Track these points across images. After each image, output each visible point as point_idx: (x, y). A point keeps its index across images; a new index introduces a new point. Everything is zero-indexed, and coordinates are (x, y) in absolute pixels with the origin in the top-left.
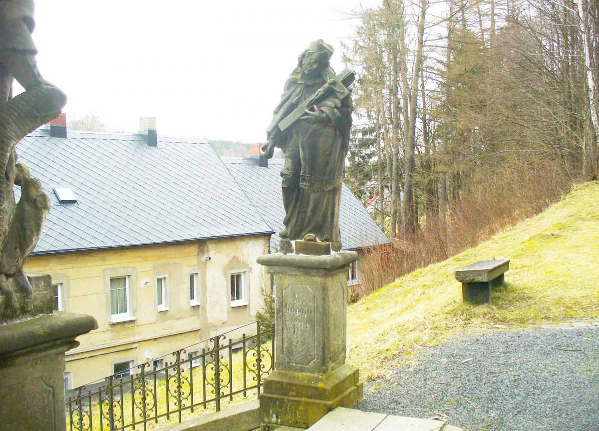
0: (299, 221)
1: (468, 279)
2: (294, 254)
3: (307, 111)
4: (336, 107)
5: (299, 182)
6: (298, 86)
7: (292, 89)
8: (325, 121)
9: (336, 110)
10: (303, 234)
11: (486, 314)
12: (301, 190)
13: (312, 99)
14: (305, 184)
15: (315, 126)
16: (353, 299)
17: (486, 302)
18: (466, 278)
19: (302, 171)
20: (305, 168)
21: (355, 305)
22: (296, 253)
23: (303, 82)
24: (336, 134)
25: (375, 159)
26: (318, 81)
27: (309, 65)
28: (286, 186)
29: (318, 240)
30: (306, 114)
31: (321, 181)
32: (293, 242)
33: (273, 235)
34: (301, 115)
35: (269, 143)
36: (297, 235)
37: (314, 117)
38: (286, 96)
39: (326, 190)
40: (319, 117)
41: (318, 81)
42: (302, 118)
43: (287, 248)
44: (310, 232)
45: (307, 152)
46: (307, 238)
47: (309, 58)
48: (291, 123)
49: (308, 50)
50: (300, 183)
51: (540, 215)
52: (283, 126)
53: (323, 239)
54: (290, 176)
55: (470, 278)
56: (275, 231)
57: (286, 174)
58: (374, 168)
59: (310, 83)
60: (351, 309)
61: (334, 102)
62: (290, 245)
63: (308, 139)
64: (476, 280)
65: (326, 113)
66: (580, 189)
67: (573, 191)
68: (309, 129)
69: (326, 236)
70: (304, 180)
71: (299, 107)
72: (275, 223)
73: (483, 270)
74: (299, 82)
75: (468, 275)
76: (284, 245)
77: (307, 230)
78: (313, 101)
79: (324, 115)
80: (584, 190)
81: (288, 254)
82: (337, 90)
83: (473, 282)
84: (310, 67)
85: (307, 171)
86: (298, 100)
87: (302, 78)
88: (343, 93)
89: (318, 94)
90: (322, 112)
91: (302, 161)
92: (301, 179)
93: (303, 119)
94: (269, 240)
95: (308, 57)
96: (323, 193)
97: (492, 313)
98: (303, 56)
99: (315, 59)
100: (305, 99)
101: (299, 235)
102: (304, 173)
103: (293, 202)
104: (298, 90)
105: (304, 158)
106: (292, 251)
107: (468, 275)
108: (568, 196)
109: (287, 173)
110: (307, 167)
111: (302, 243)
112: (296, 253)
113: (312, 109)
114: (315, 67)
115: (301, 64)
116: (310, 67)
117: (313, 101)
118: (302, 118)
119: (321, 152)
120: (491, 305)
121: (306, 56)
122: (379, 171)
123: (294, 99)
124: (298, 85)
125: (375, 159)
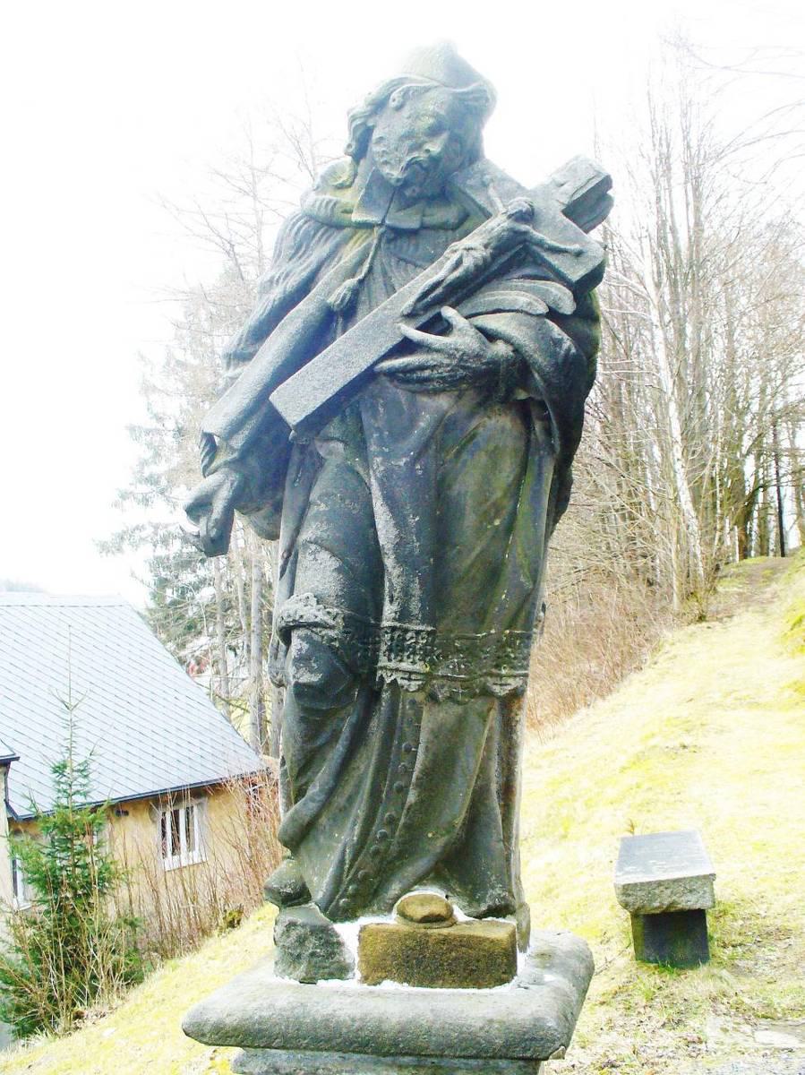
0: (378, 830)
1: (656, 904)
2: (353, 983)
3: (417, 335)
4: (553, 314)
5: (377, 661)
6: (346, 241)
7: (319, 251)
8: (495, 382)
9: (556, 331)
10: (395, 888)
11: (714, 1000)
12: (385, 695)
13: (435, 278)
14: (405, 665)
15: (444, 402)
16: (230, 919)
17: (704, 963)
18: (651, 901)
19: (389, 610)
20: (406, 593)
21: (237, 934)
22: (365, 979)
23: (373, 218)
24: (528, 441)
25: (206, 594)
26: (448, 214)
27: (408, 143)
28: (315, 678)
29: (460, 915)
30: (406, 346)
31: (472, 651)
32: (348, 932)
33: (13, 764)
34: (384, 350)
35: (220, 486)
36: (360, 893)
37: (451, 356)
38: (277, 293)
39: (497, 689)
40: (478, 356)
41: (441, 215)
42: (387, 364)
43: (315, 957)
44: (420, 880)
45: (413, 521)
46: (420, 912)
47: (406, 112)
48: (336, 388)
49: (401, 81)
50: (383, 661)
51: (612, 700)
52: (297, 400)
53: (483, 908)
54: (332, 633)
55: (658, 903)
56: (17, 756)
57: (316, 625)
58: (208, 609)
59: (410, 220)
60: (232, 948)
61: (543, 295)
62: (332, 945)
63: (415, 460)
64: (680, 906)
65: (508, 341)
66: (679, 641)
67: (667, 647)
68: (413, 421)
69: (494, 895)
70: (398, 649)
71: (374, 312)
72: (17, 736)
73: (698, 878)
74: (356, 217)
75: (657, 891)
76: (301, 941)
77: (411, 871)
78: (439, 290)
79: (501, 349)
80: (690, 642)
81: (321, 983)
82: (550, 242)
83: (672, 910)
84: (412, 149)
85: (415, 606)
86: (356, 292)
87: (367, 202)
88: (579, 254)
89: (459, 263)
90: (490, 336)
91: (389, 562)
92: (384, 648)
93: (392, 374)
94: (6, 774)
95: (399, 108)
96: (478, 704)
97: (732, 993)
98: (379, 106)
99: (435, 115)
100: (390, 289)
101: (376, 894)
102: (403, 615)
103: (340, 747)
104: (350, 254)
105: (400, 545)
106: (341, 971)
107: (657, 891)
108: (661, 658)
109: (322, 617)
110: (416, 589)
111: (391, 935)
112: (365, 979)
113: (439, 326)
114: (435, 147)
115: (361, 145)
116: (412, 149)
117: (439, 290)
118: (387, 364)
119: (470, 520)
120: (715, 971)
121: (392, 104)
122: (218, 616)
123: (330, 289)
124: (347, 231)
125: (206, 594)
